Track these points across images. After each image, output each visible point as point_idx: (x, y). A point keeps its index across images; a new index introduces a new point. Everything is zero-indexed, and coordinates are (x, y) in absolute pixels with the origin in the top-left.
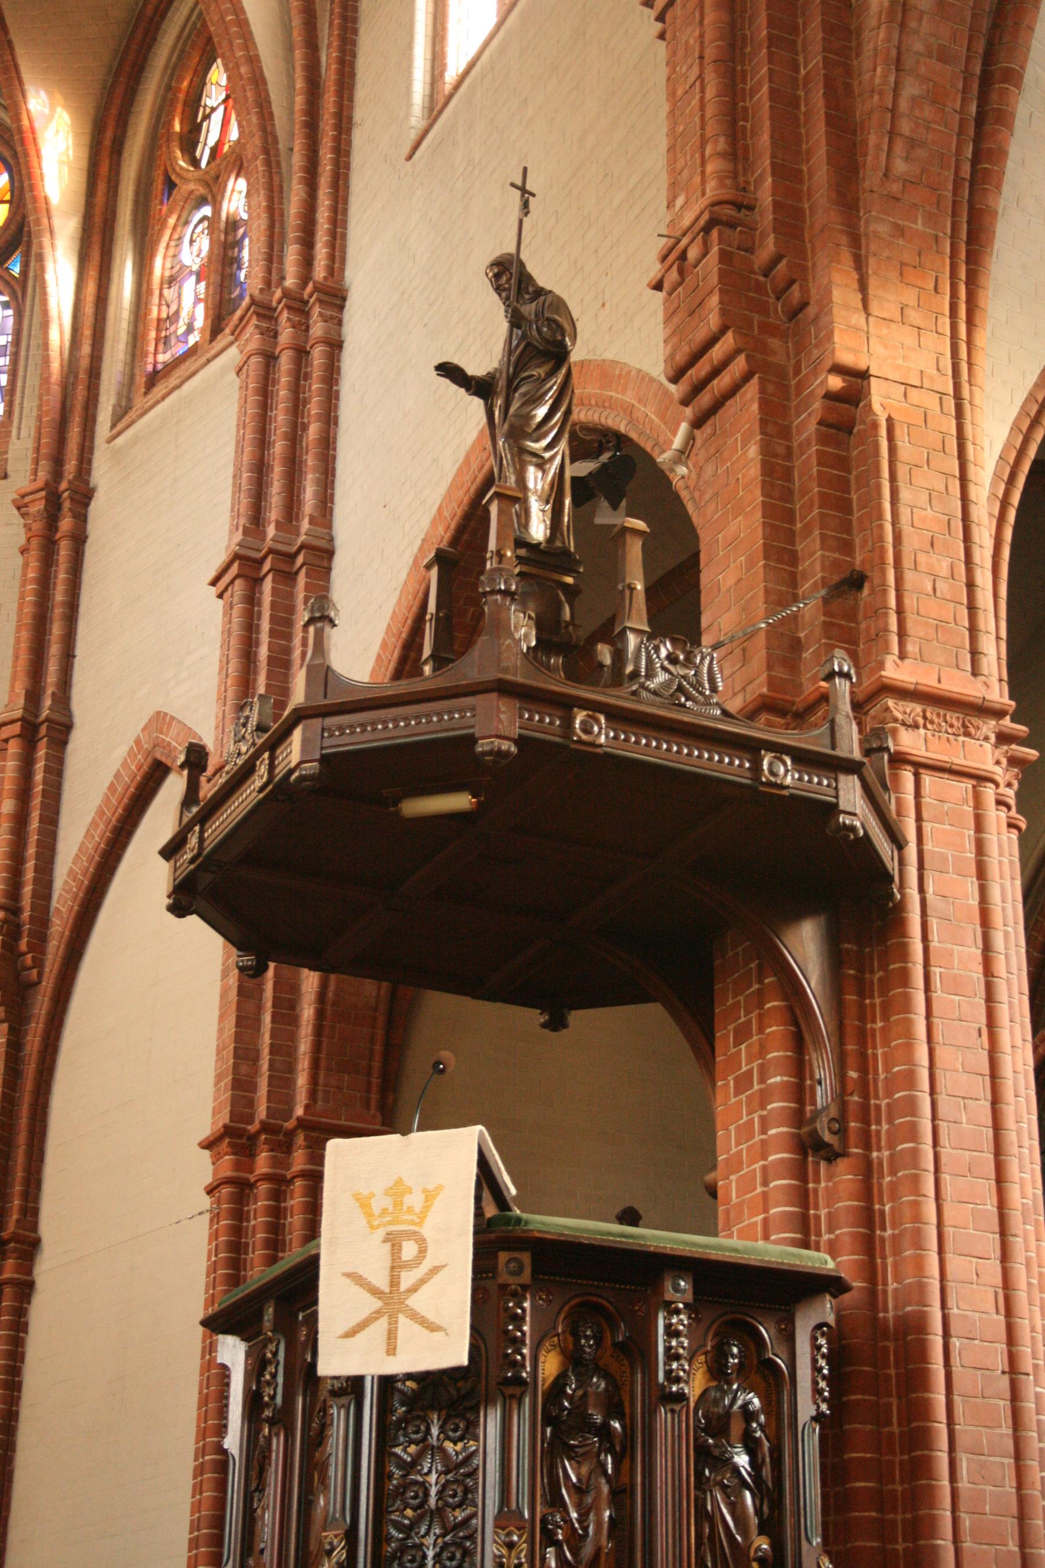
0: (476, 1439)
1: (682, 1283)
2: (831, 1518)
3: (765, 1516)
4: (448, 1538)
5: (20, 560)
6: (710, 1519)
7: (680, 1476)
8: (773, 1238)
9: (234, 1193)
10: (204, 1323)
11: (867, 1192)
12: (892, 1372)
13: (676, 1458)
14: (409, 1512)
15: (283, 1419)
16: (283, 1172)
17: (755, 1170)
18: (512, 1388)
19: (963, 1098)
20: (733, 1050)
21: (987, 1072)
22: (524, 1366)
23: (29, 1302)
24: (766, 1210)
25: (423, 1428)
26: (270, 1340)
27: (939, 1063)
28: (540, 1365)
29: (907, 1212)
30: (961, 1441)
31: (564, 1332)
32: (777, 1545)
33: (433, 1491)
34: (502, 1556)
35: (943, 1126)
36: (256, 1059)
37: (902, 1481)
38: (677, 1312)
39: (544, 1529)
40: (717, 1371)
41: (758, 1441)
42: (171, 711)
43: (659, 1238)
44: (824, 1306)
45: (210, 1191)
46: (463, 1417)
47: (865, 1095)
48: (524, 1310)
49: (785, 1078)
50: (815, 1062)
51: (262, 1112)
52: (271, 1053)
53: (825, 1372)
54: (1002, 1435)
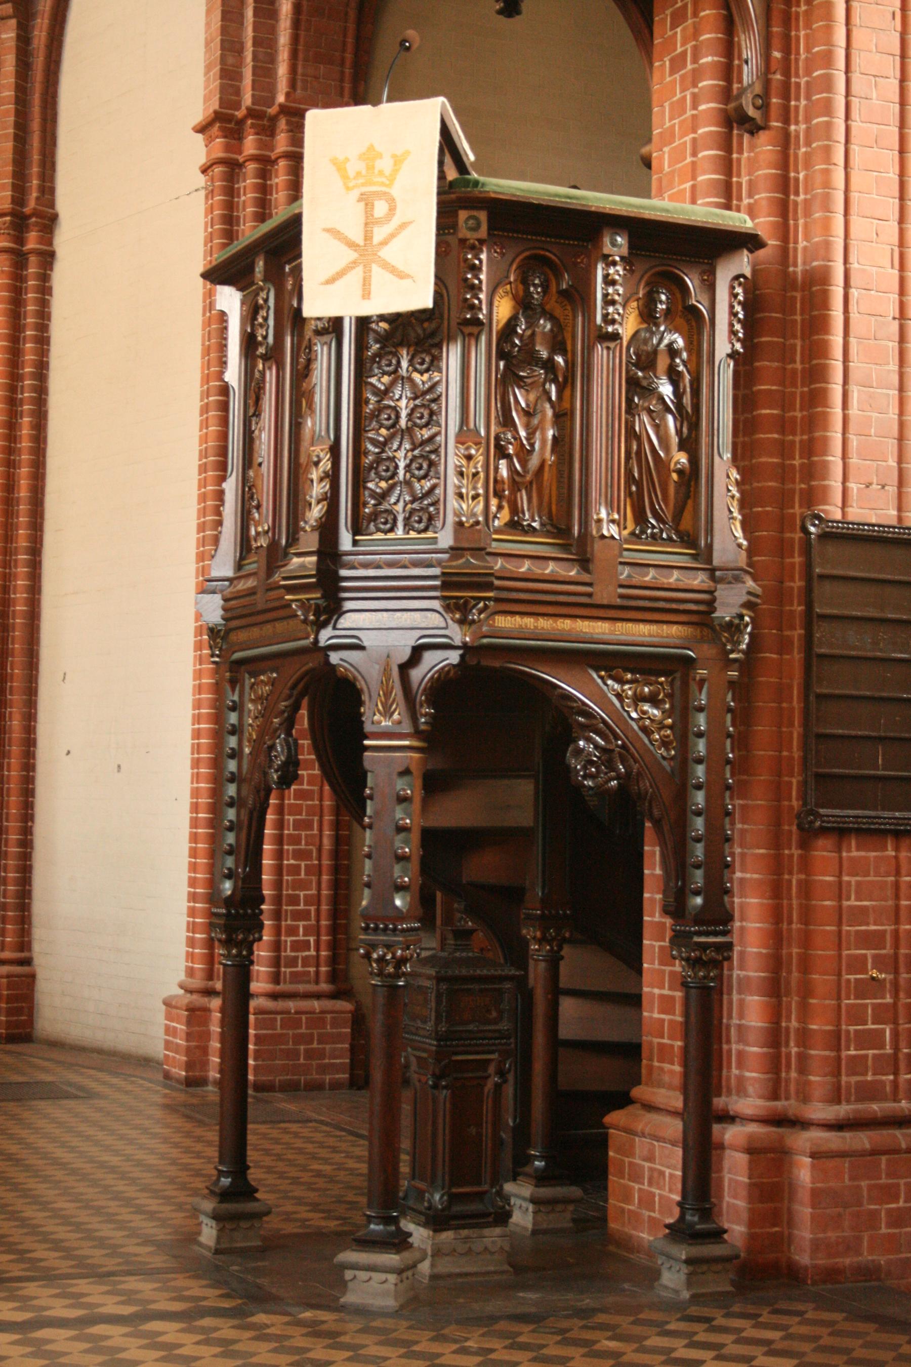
0: (440, 370)
1: (619, 239)
2: (741, 439)
3: (685, 435)
4: (416, 452)
6: (638, 438)
7: (613, 394)
8: (699, 202)
9: (227, 171)
10: (206, 276)
11: (784, 161)
12: (798, 318)
13: (610, 387)
14: (383, 431)
15: (274, 355)
16: (268, 153)
17: (685, 143)
18: (472, 327)
19: (875, 76)
20: (670, 33)
21: (898, 52)
22: (480, 309)
23: (51, 269)
24: (694, 178)
25: (394, 362)
26: (262, 289)
27: (855, 44)
28: (495, 309)
29: (818, 179)
30: (853, 375)
31: (515, 280)
32: (694, 460)
33: (404, 414)
34: (461, 467)
35: (855, 101)
36: (240, 51)
37: (801, 410)
38: (614, 263)
39: (498, 446)
40: (648, 315)
41: (680, 374)
43: (600, 199)
44: (742, 261)
45: (204, 170)
46: (428, 352)
47: (787, 73)
48: (481, 261)
49: (716, 59)
50: (743, 43)
51: (247, 99)
52: (254, 45)
53: (741, 335)
54: (889, 371)
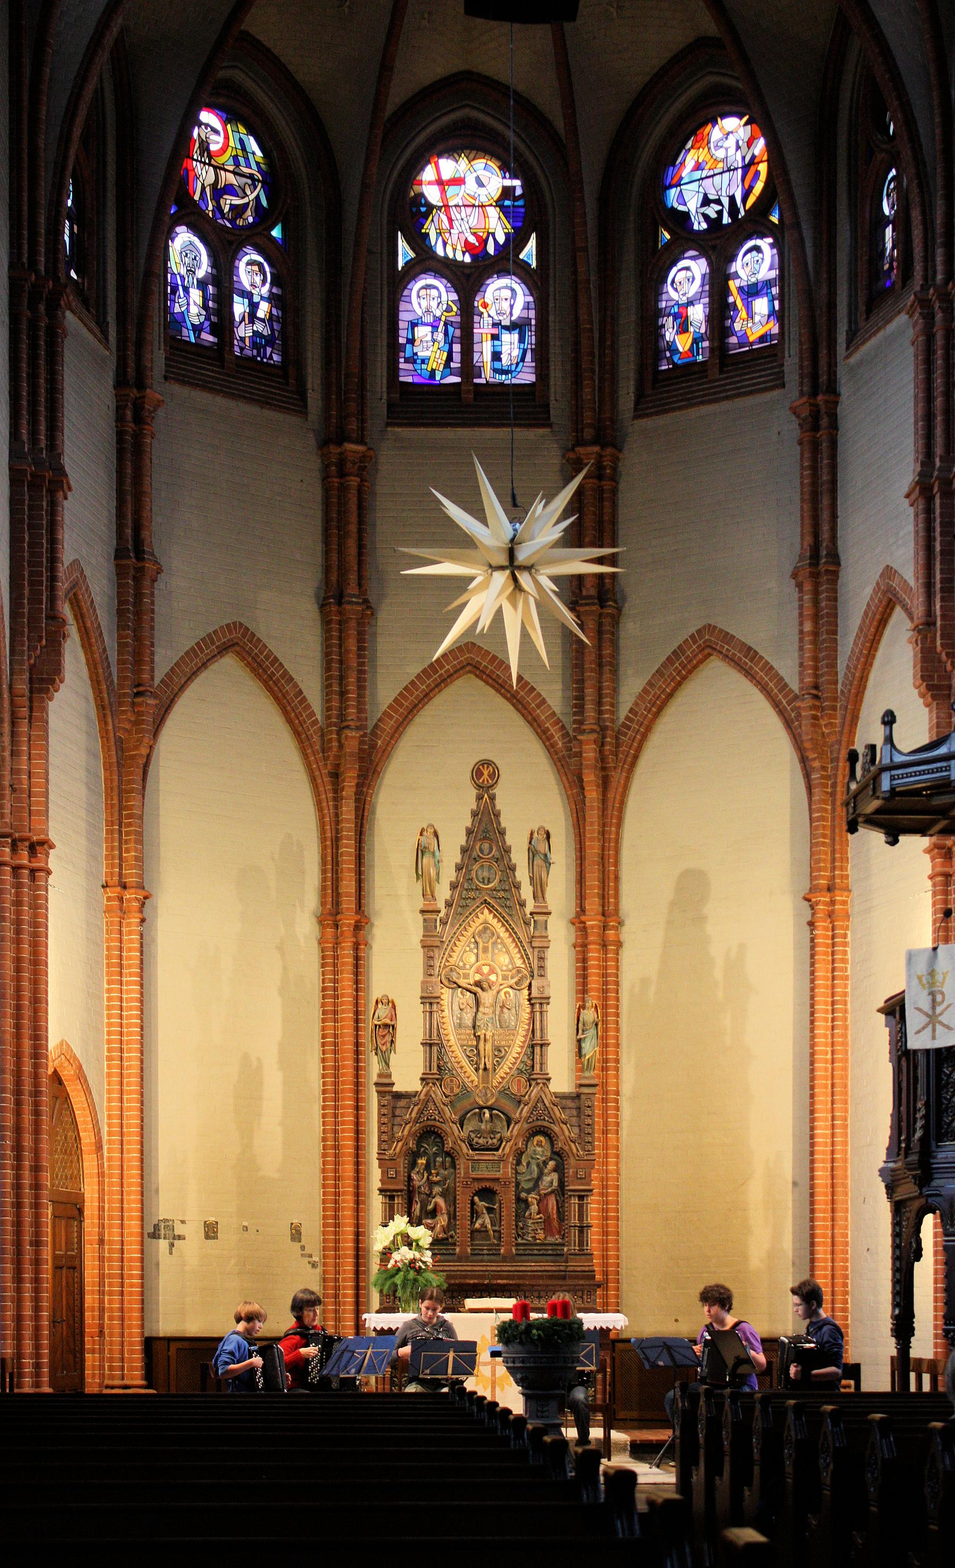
5: (799, 448)
42: (895, 567)
